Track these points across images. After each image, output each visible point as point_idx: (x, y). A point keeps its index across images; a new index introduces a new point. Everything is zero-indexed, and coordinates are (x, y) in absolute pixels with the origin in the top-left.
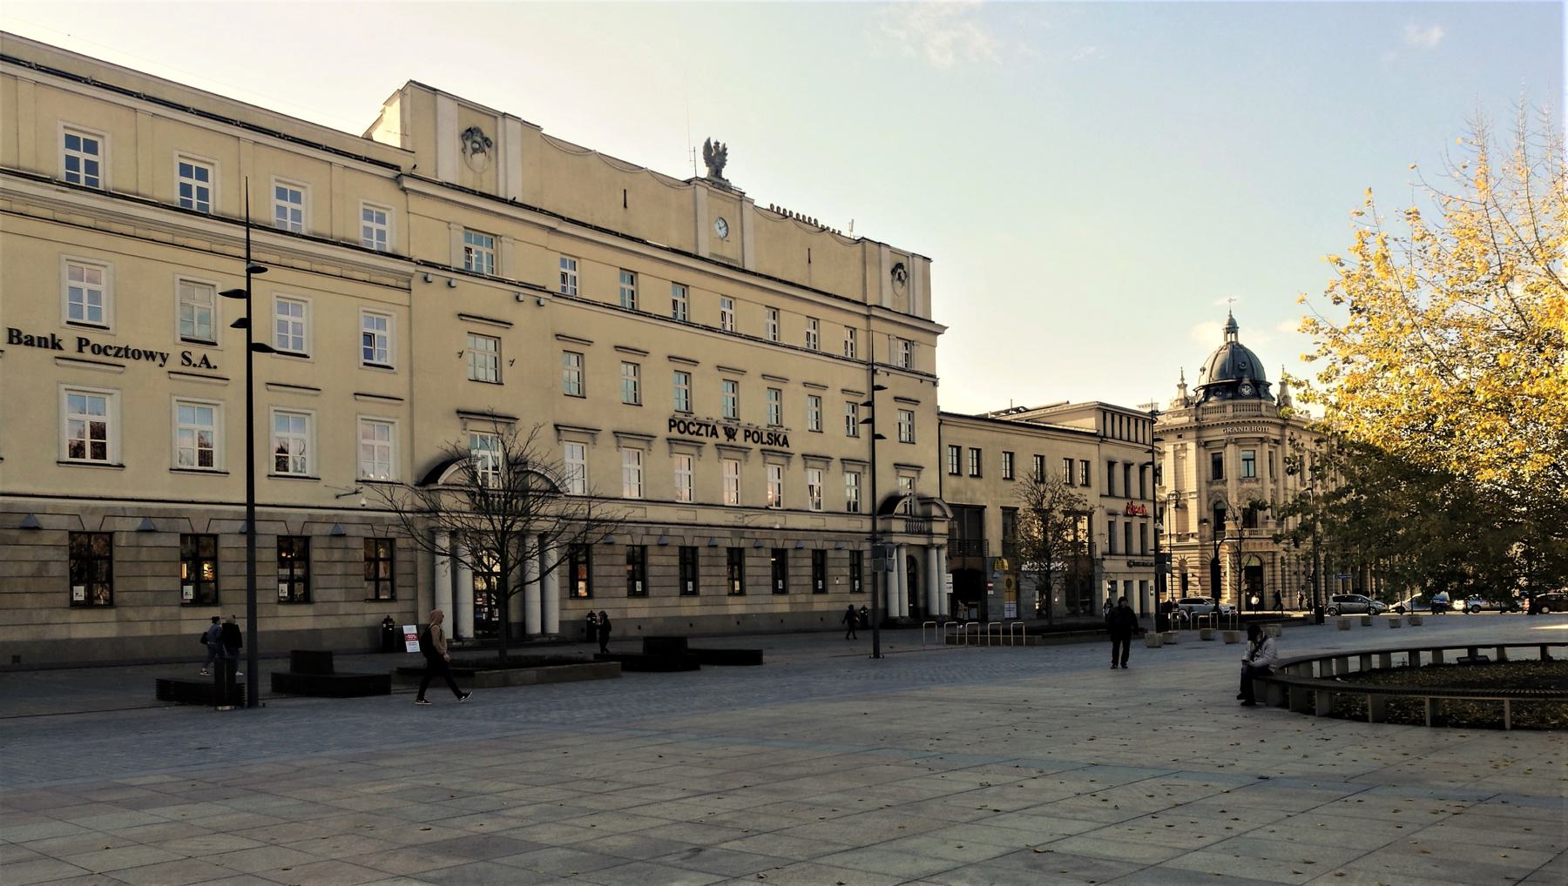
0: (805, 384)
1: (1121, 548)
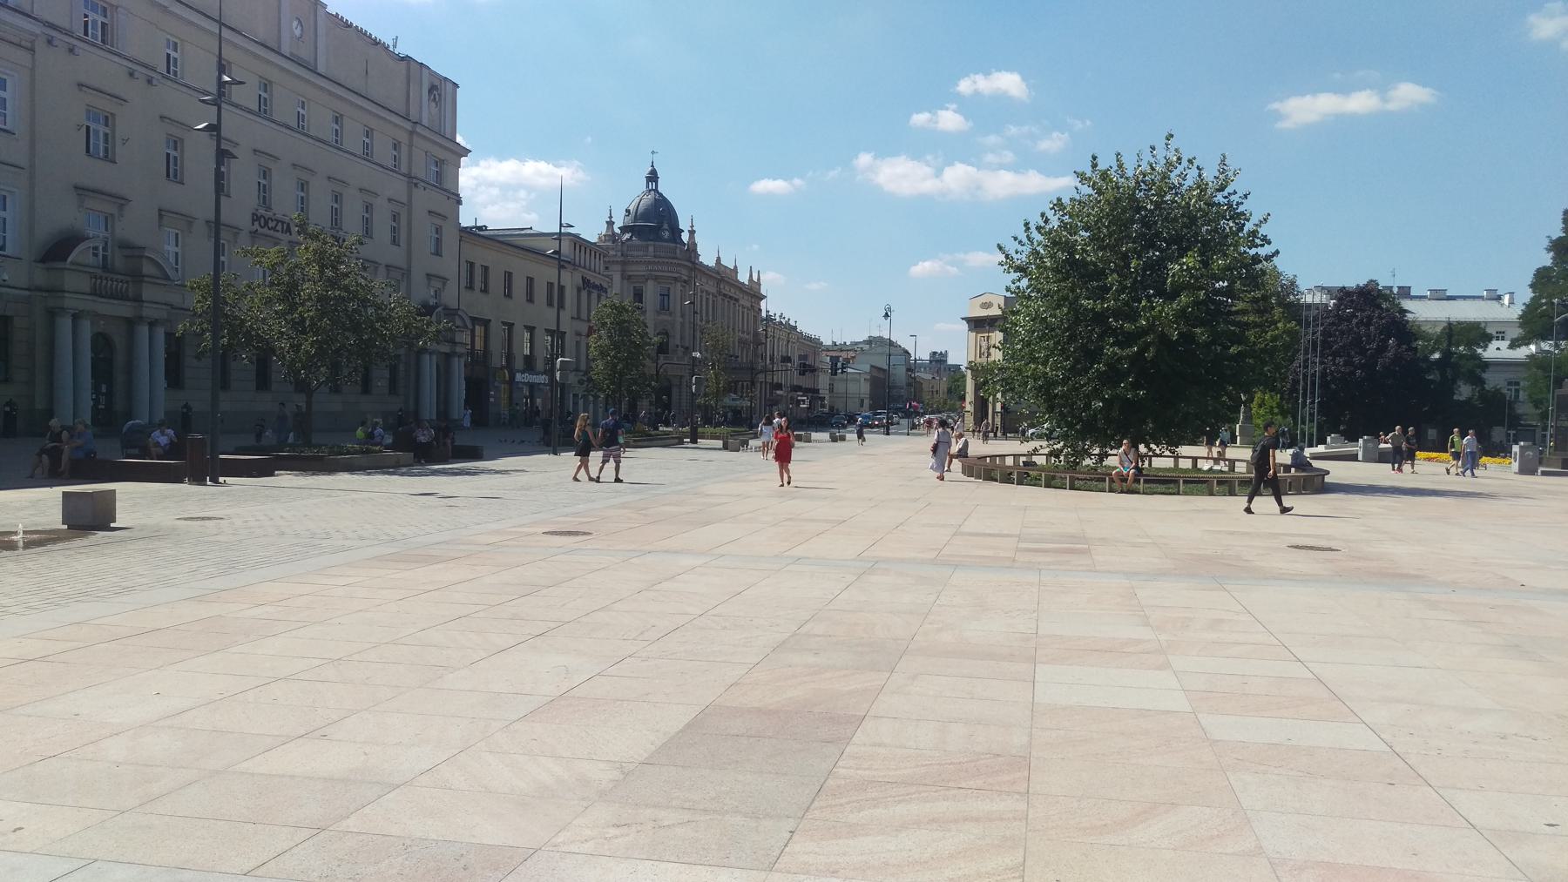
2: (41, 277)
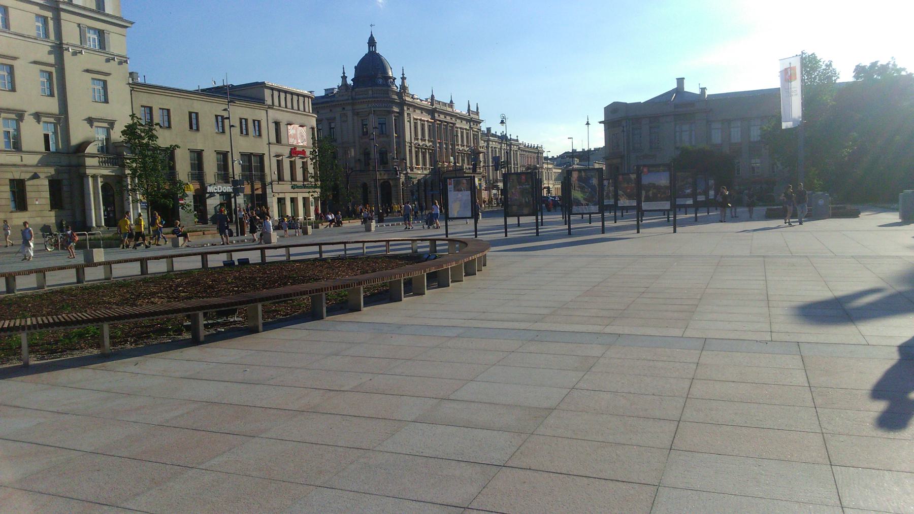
1: (287, 175)
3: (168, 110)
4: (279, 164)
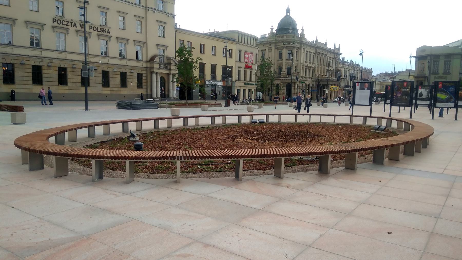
0: (118, 12)
1: (242, 78)
2: (149, 65)
3: (191, 43)
4: (239, 71)
